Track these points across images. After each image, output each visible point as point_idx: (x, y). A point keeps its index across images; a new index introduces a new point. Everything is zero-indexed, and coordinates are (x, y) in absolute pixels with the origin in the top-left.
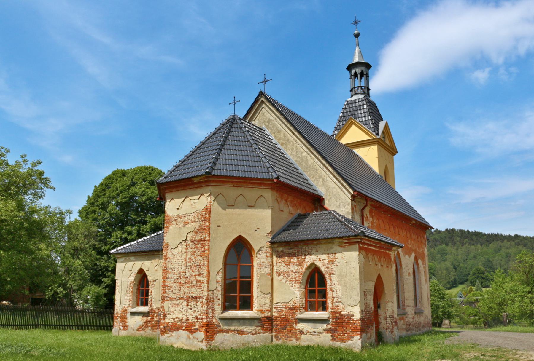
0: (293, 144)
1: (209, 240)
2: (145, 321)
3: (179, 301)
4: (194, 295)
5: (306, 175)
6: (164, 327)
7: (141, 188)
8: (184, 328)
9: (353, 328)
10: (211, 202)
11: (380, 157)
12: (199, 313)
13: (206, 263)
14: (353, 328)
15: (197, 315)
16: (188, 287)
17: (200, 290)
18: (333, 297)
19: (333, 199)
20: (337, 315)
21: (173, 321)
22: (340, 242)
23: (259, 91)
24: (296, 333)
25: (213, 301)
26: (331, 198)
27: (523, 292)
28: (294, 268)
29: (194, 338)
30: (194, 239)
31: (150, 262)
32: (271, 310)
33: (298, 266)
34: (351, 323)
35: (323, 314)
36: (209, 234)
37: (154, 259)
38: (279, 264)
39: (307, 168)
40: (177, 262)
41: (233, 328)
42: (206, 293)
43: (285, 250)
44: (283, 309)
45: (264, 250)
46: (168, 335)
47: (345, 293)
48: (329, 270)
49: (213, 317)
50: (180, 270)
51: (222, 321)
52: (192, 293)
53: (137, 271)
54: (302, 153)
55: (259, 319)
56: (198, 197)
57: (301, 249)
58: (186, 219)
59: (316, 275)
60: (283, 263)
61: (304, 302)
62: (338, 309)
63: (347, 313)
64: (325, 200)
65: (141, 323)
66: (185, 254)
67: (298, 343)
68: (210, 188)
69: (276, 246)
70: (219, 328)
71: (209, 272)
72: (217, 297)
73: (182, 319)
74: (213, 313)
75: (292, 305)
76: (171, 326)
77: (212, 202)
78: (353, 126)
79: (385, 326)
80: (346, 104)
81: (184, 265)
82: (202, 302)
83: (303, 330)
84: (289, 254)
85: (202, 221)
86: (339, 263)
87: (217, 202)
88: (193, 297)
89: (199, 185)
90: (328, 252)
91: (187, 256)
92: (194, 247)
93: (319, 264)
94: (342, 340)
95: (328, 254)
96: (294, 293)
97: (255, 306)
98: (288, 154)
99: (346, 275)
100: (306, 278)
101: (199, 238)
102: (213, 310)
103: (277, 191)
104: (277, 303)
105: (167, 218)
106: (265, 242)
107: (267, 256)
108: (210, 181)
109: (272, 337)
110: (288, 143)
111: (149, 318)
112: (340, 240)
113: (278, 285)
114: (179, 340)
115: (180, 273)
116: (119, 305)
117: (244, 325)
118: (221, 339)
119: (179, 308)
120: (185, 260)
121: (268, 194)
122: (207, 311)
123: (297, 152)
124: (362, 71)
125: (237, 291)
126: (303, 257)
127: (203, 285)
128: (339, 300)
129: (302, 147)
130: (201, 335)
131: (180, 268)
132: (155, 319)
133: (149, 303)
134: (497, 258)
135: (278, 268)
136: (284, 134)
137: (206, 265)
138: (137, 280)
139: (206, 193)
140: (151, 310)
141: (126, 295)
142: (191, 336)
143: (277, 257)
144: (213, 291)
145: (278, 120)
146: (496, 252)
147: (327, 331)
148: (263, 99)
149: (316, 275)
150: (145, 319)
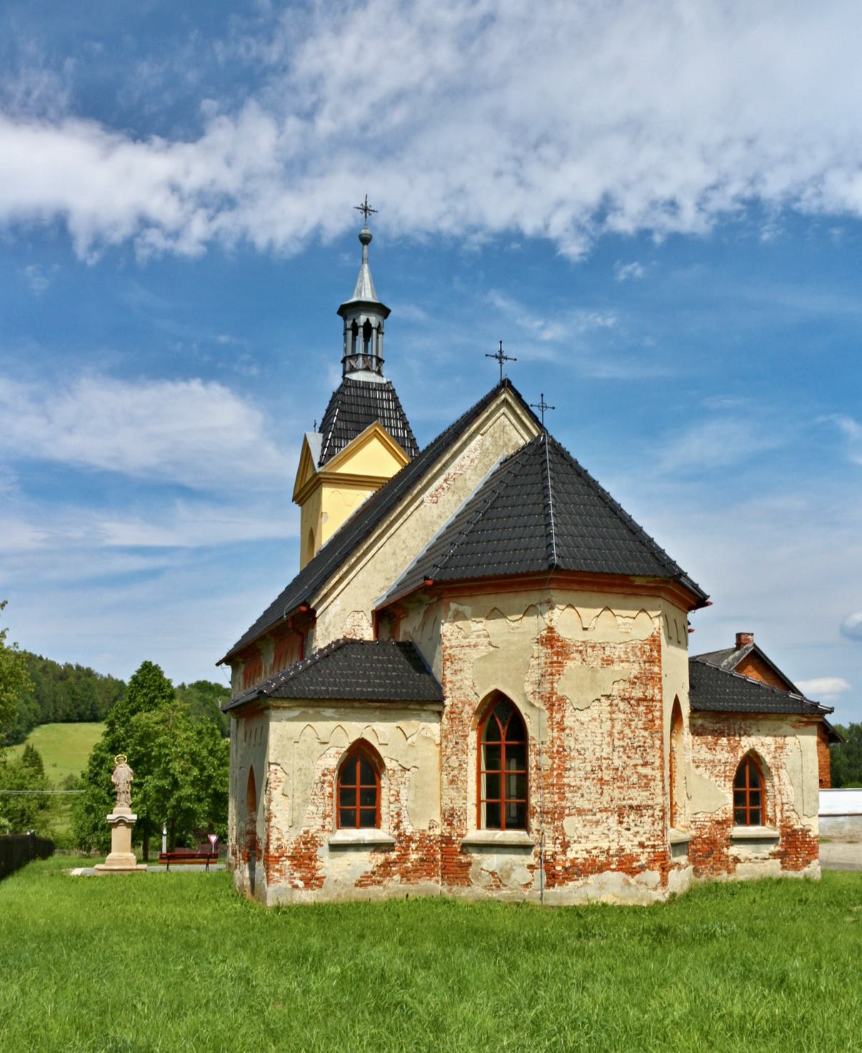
2: (379, 862)
3: (599, 816)
4: (635, 803)
6: (566, 869)
8: (613, 867)
12: (647, 836)
13: (658, 743)
15: (643, 839)
16: (619, 787)
17: (648, 793)
20: (789, 830)
21: (587, 856)
24: (728, 861)
30: (627, 695)
31: (395, 724)
33: (727, 753)
40: (590, 738)
43: (707, 724)
44: (706, 823)
48: (777, 762)
50: (598, 755)
52: (630, 799)
53: (347, 746)
56: (634, 613)
57: (735, 724)
58: (607, 653)
60: (703, 745)
62: (789, 821)
63: (802, 827)
65: (370, 868)
66: (609, 723)
67: (732, 878)
73: (609, 849)
76: (584, 865)
78: (375, 442)
81: (608, 744)
82: (653, 816)
83: (739, 857)
85: (645, 662)
88: (631, 807)
90: (776, 733)
91: (613, 727)
93: (762, 751)
94: (796, 868)
95: (775, 736)
96: (724, 797)
101: (640, 695)
104: (695, 814)
105: (559, 644)
111: (393, 855)
114: (609, 889)
116: (285, 829)
119: (601, 828)
120: (611, 735)
126: (737, 738)
127: (652, 783)
131: (598, 749)
132: (414, 856)
135: (695, 755)
137: (658, 746)
139: (652, 610)
140: (400, 835)
147: (775, 855)
150: (380, 858)
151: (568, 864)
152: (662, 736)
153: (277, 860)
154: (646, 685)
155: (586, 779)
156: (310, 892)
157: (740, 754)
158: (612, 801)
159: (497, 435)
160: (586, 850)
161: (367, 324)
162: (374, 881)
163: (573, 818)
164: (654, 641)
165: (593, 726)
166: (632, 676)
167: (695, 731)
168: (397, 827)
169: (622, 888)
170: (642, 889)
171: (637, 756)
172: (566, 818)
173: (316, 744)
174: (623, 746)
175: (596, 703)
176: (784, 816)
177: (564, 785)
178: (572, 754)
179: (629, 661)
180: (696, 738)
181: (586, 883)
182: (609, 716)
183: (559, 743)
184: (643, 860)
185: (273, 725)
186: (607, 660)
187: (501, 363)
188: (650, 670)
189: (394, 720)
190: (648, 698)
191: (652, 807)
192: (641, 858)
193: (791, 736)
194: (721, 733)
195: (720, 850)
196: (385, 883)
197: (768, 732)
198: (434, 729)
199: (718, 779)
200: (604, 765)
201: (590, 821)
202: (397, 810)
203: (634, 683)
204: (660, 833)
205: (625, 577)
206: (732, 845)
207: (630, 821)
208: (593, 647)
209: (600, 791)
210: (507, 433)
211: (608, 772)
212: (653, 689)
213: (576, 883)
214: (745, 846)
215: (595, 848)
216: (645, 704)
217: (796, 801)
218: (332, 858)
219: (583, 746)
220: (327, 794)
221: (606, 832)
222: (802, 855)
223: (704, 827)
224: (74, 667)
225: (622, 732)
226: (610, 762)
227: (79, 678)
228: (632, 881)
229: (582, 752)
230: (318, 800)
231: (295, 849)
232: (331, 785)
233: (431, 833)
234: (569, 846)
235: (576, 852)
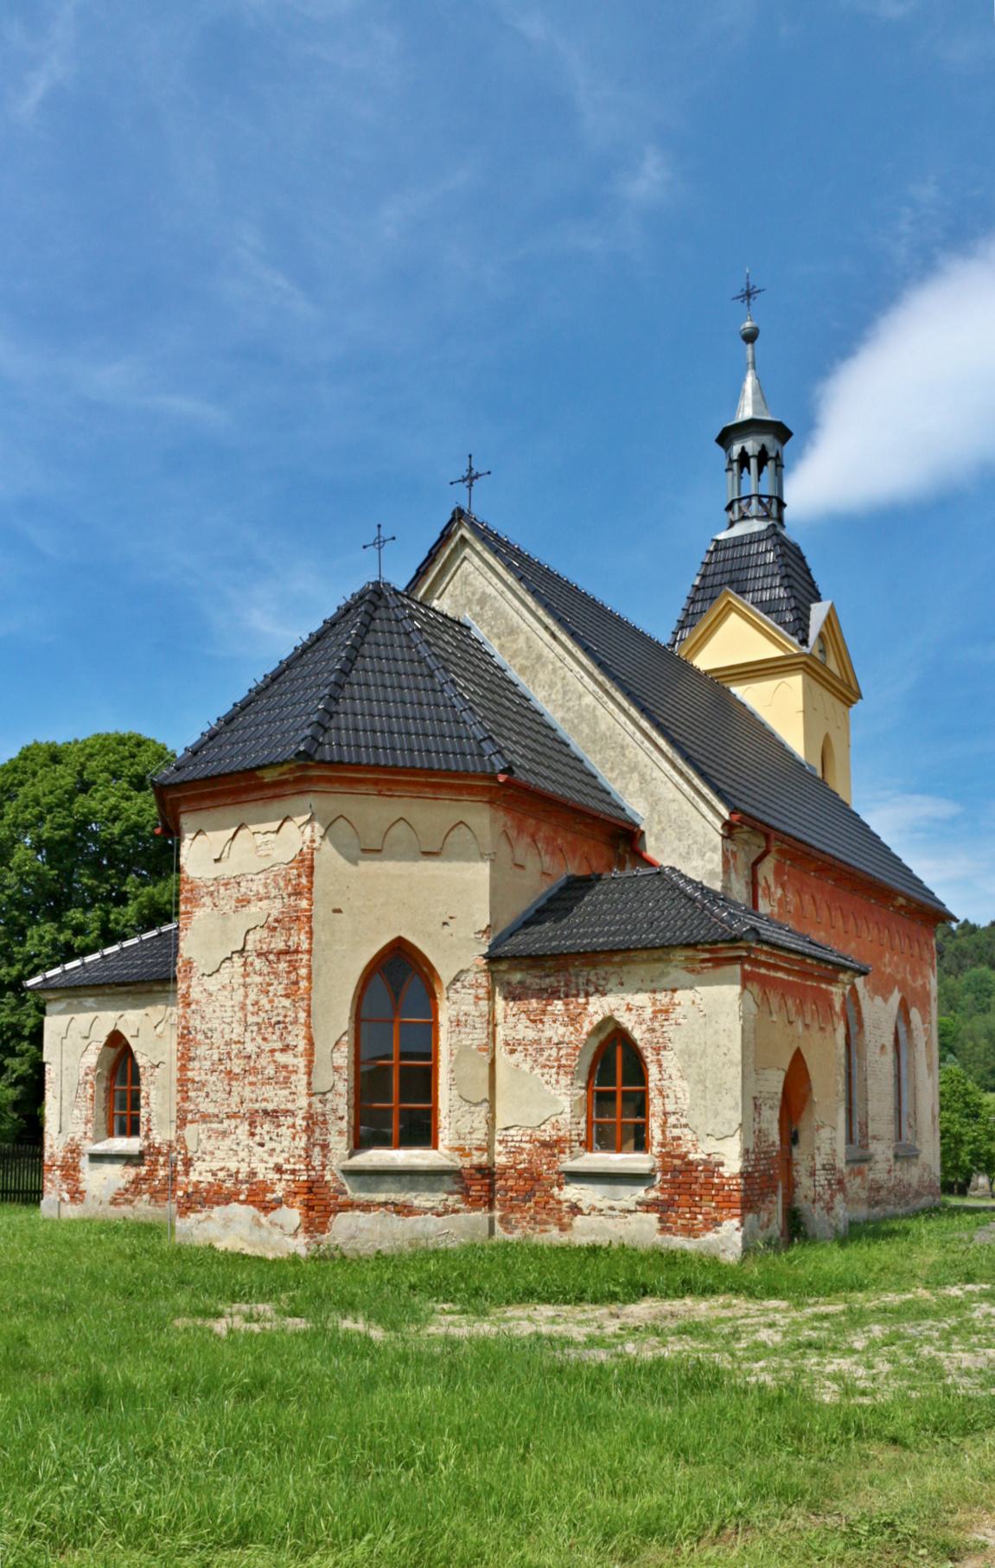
0: (554, 671)
1: (309, 952)
3: (226, 1122)
4: (270, 1107)
5: (593, 761)
7: (106, 798)
8: (242, 1197)
10: (313, 841)
11: (809, 711)
12: (286, 1155)
13: (302, 1016)
14: (719, 1199)
15: (281, 1160)
16: (251, 1084)
17: (286, 1092)
19: (671, 834)
20: (677, 1162)
21: (211, 1179)
22: (687, 958)
23: (454, 506)
24: (560, 1210)
25: (325, 1122)
26: (664, 830)
28: (555, 1031)
31: (142, 1012)
32: (488, 1148)
33: (568, 1025)
36: (310, 933)
37: (153, 1003)
38: (511, 1019)
39: (594, 742)
40: (218, 1014)
41: (381, 1197)
42: (303, 1102)
43: (529, 980)
45: (469, 978)
48: (657, 1038)
49: (324, 1166)
50: (227, 1037)
51: (352, 1178)
52: (265, 1100)
53: (104, 1039)
54: (580, 697)
56: (275, 825)
57: (577, 976)
58: (243, 890)
59: (619, 1050)
60: (523, 1016)
61: (583, 1125)
63: (704, 1157)
65: (122, 1183)
68: (309, 799)
69: (503, 967)
70: (342, 1199)
71: (310, 1041)
72: (334, 1111)
74: (325, 1156)
75: (548, 1134)
76: (208, 1191)
77: (318, 840)
78: (734, 618)
82: (293, 1126)
83: (580, 1204)
85: (290, 895)
86: (685, 1017)
88: (266, 1112)
89: (277, 791)
90: (654, 985)
91: (246, 996)
92: (266, 970)
93: (627, 1020)
94: (690, 1231)
95: (654, 991)
96: (555, 1102)
98: (540, 698)
99: (704, 1052)
100: (588, 1059)
101: (282, 946)
102: (325, 1147)
105: (188, 887)
106: (473, 954)
107: (477, 998)
108: (310, 780)
109: (491, 1221)
110: (538, 666)
111: (143, 1170)
112: (689, 953)
113: (509, 1077)
114: (230, 1230)
115: (227, 1044)
116: (55, 1134)
117: (412, 1189)
118: (343, 1226)
119: (228, 1142)
120: (243, 1007)
121: (481, 818)
122: (306, 1150)
123: (565, 693)
124: (763, 447)
126: (582, 1000)
127: (293, 1077)
128: (683, 1121)
129: (580, 680)
130: (292, 1216)
131: (227, 1030)
132: (161, 1173)
133: (143, 1129)
136: (528, 639)
139: (300, 814)
141: (74, 1105)
142: (264, 1220)
143: (505, 998)
145: (509, 596)
147: (648, 1206)
148: (464, 532)
149: (619, 1050)
150: (132, 1172)
151: (190, 1190)
157: (587, 1027)
161: (743, 453)
168: (147, 1137)
170: (277, 1235)
176: (669, 1135)
181: (209, 1217)
189: (143, 1006)
194: (553, 993)
197: (639, 985)
201: (216, 1131)
203: (275, 929)
205: (249, 772)
210: (471, 585)
217: (691, 1108)
228: (264, 1220)
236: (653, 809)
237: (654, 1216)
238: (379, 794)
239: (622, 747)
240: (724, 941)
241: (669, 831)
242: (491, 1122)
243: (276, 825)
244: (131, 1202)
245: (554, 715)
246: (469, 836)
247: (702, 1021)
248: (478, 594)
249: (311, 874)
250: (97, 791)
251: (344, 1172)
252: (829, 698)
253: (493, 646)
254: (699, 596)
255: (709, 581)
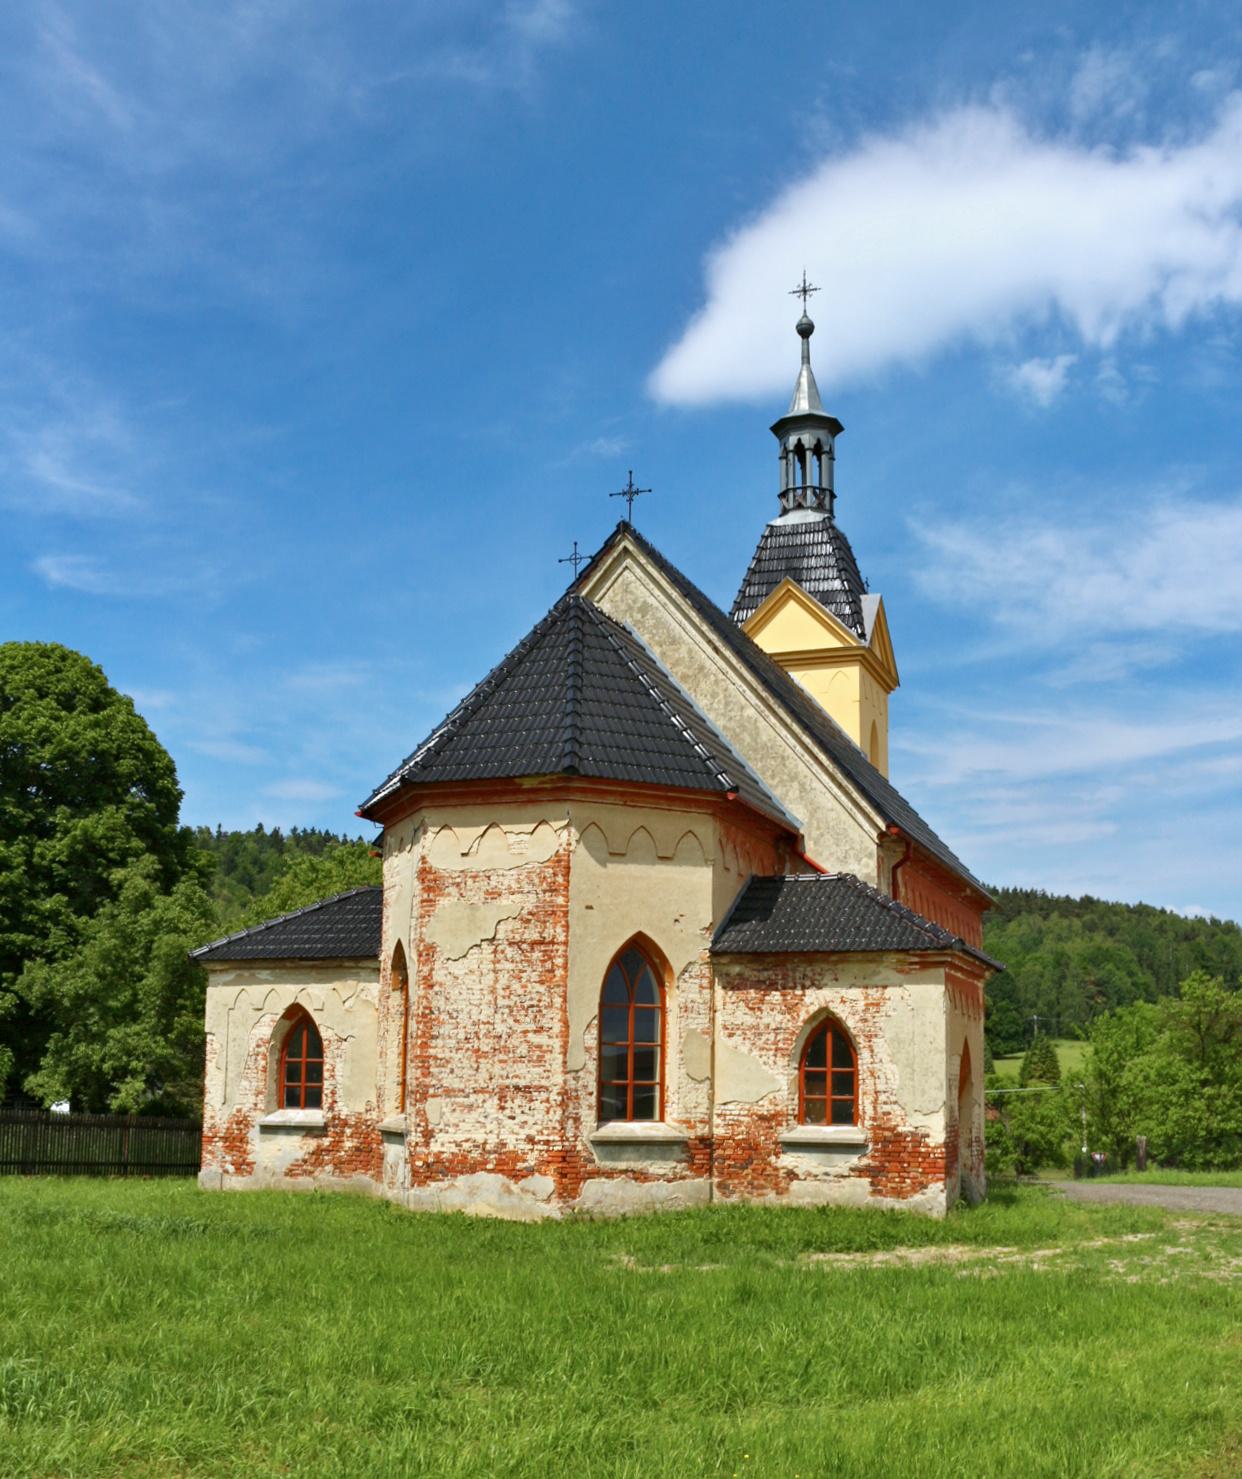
0: (716, 682)
1: (566, 943)
2: (311, 1149)
3: (473, 1098)
4: (522, 1083)
5: (755, 767)
7: (34, 718)
9: (925, 1165)
10: (569, 844)
11: (865, 700)
12: (539, 1127)
13: (558, 1001)
14: (925, 1165)
15: (533, 1132)
16: (501, 1061)
17: (541, 1069)
18: (876, 1092)
19: (828, 839)
20: (887, 1134)
21: (455, 1150)
22: (899, 961)
23: (619, 520)
24: (777, 1176)
25: (577, 1097)
26: (822, 835)
27: (1192, 1081)
29: (524, 1190)
30: (518, 938)
32: (708, 1122)
33: (784, 1014)
34: (920, 1153)
35: (849, 1132)
36: (567, 927)
37: (340, 978)
38: (729, 1006)
39: (755, 750)
40: (464, 996)
41: (622, 1165)
42: (559, 1079)
43: (747, 973)
45: (695, 970)
46: (440, 1184)
47: (907, 1082)
49: (576, 1137)
50: (475, 1018)
51: (600, 1148)
52: (517, 1076)
53: (281, 1012)
54: (742, 708)
55: (682, 1144)
56: (530, 827)
57: (794, 971)
58: (493, 883)
59: (829, 1036)
60: (741, 1003)
61: (796, 1101)
63: (913, 1130)
64: (806, 838)
65: (300, 1155)
66: (492, 975)
68: (567, 807)
69: (724, 960)
70: (590, 1167)
71: (566, 1023)
72: (585, 1087)
73: (485, 1143)
74: (577, 1128)
75: (766, 1108)
76: (451, 1162)
77: (574, 843)
78: (792, 605)
79: (969, 1163)
80: (767, 533)
82: (548, 1101)
83: (796, 1171)
84: (759, 981)
85: (545, 891)
86: (894, 1010)
87: (585, 844)
88: (517, 1088)
89: (532, 796)
90: (866, 982)
91: (496, 981)
92: (518, 958)
93: (841, 1011)
94: (899, 1193)
95: (866, 987)
96: (774, 1080)
97: (673, 1112)
98: (701, 704)
99: (912, 1040)
100: (802, 1043)
101: (536, 937)
102: (577, 1120)
103: (722, 820)
104: (725, 1104)
105: (431, 877)
106: (701, 948)
107: (701, 987)
108: (567, 789)
109: (711, 1184)
110: (700, 676)
111: (326, 1142)
112: (901, 956)
113: (728, 1057)
114: (480, 1196)
115: (474, 1024)
116: (218, 1106)
117: (648, 1158)
118: (595, 1193)
119: (475, 1115)
120: (493, 991)
121: (706, 829)
122: (562, 1123)
123: (727, 704)
124: (819, 441)
125: (629, 1079)
126: (799, 992)
127: (548, 1056)
128: (893, 1099)
129: (743, 694)
130: (547, 1183)
131: (475, 1011)
132: (348, 1144)
133: (326, 1101)
134: (1029, 966)
136: (690, 651)
137: (558, 1005)
138: (279, 1037)
139: (555, 820)
140: (334, 1118)
141: (241, 1076)
143: (724, 988)
144: (577, 1071)
145: (672, 608)
146: (1027, 949)
147: (860, 1172)
148: (628, 544)
149: (829, 1036)
150: (312, 1144)
151: (431, 1159)
152: (565, 992)
153: (211, 1140)
154: (545, 922)
155: (457, 1050)
156: (240, 1178)
157: (803, 1016)
158: (491, 1079)
159: (618, 598)
160: (455, 1142)
162: (305, 1171)
163: (438, 1100)
164: (559, 861)
165: (468, 980)
166: (525, 912)
167: (728, 983)
168: (331, 1108)
169: (500, 1195)
170: (528, 1199)
171: (528, 1019)
172: (430, 1100)
173: (252, 1013)
174: (509, 1007)
175: (475, 950)
176: (880, 1110)
177: (429, 1057)
178: (442, 1017)
179: (522, 892)
180: (730, 993)
182: (491, 966)
183: (425, 1003)
184: (532, 1160)
185: (210, 990)
186: (493, 893)
187: (637, 492)
188: (551, 901)
190: (547, 940)
191: (547, 1089)
192: (528, 1157)
193: (894, 985)
195: (764, 1159)
196: (316, 1174)
197: (854, 981)
198: (373, 989)
199: (764, 1053)
200: (483, 1032)
202: (331, 1088)
203: (528, 921)
204: (557, 1125)
205: (509, 779)
206: (783, 1152)
207: (515, 1106)
208: (474, 877)
209: (475, 1066)
210: (631, 593)
211: (487, 1041)
212: (554, 927)
213: (440, 1184)
214: (806, 1155)
215: (467, 1141)
216: (543, 948)
218: (263, 1141)
219: (455, 1006)
220: (260, 1068)
221: (482, 1119)
222: (912, 1175)
223: (739, 1123)
224: (1208, 921)
225: (508, 987)
226: (491, 1027)
227: (1213, 935)
228: (514, 1187)
229: (455, 1015)
230: (252, 1074)
231: (228, 1129)
232: (265, 1058)
233: (368, 1117)
234: (433, 1137)
235: (443, 1145)
236: (812, 815)
237: (866, 1181)
238: (625, 805)
239: (783, 758)
240: (935, 948)
241: (827, 836)
242: (711, 1100)
243: (531, 827)
244: (311, 1173)
245: (717, 721)
246: (696, 844)
247: (911, 1013)
248: (632, 598)
249: (568, 873)
250: (22, 709)
251: (592, 1142)
252: (876, 687)
253: (655, 652)
254: (756, 578)
255: (765, 565)
